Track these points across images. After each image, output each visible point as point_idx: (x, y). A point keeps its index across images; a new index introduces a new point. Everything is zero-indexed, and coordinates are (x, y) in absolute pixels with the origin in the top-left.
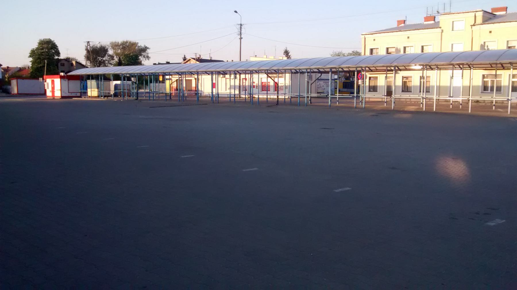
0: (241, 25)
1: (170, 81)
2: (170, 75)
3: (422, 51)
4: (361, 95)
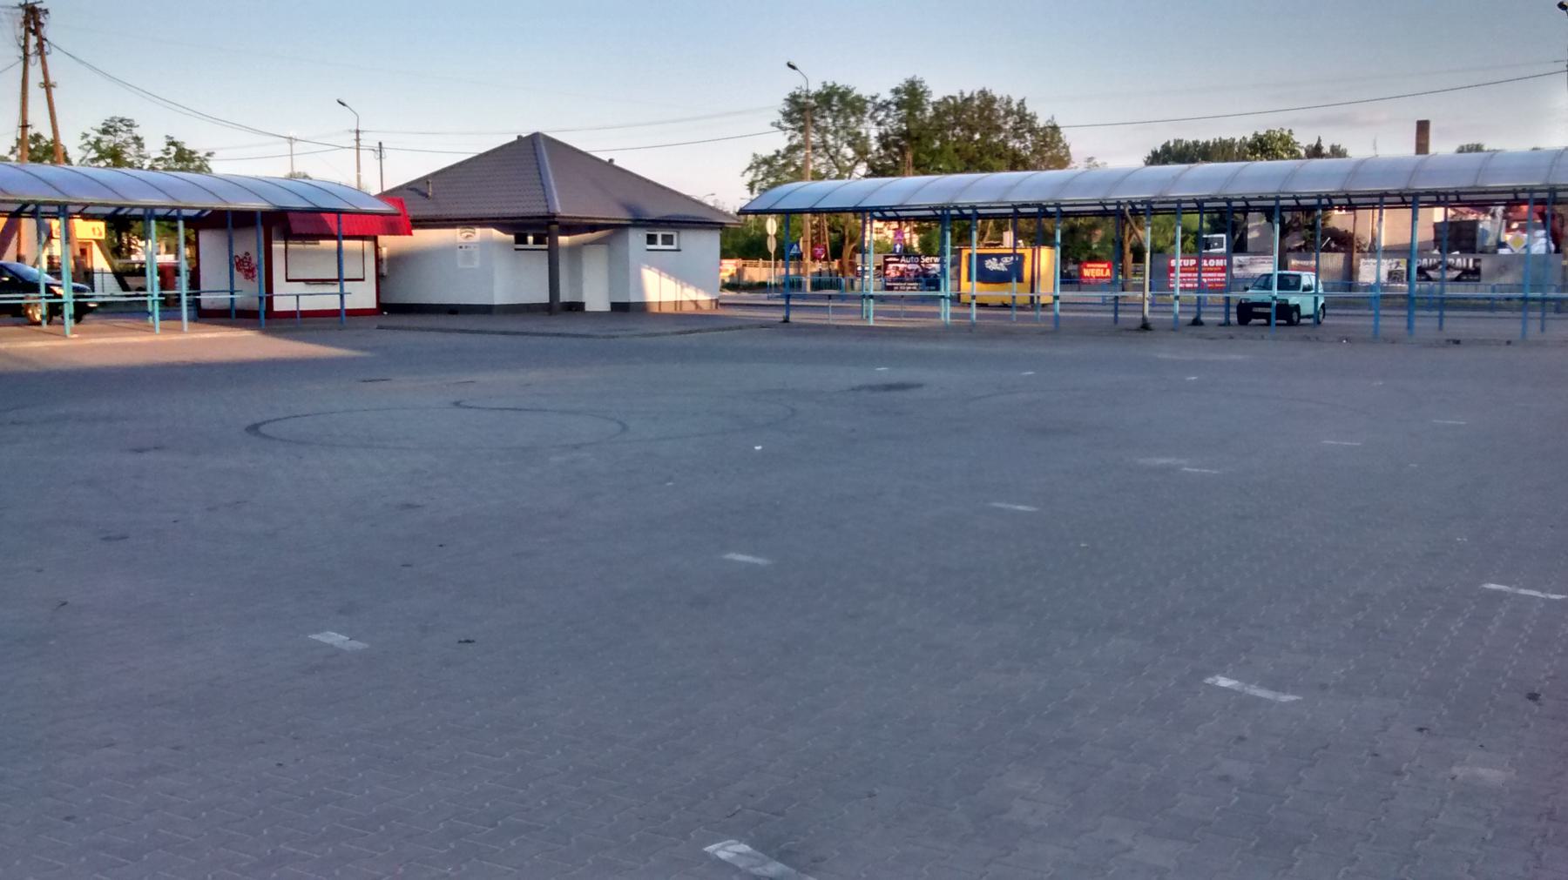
0: (358, 132)
1: (1532, 318)
2: (1351, 207)
3: (1422, 146)
4: (831, 315)
